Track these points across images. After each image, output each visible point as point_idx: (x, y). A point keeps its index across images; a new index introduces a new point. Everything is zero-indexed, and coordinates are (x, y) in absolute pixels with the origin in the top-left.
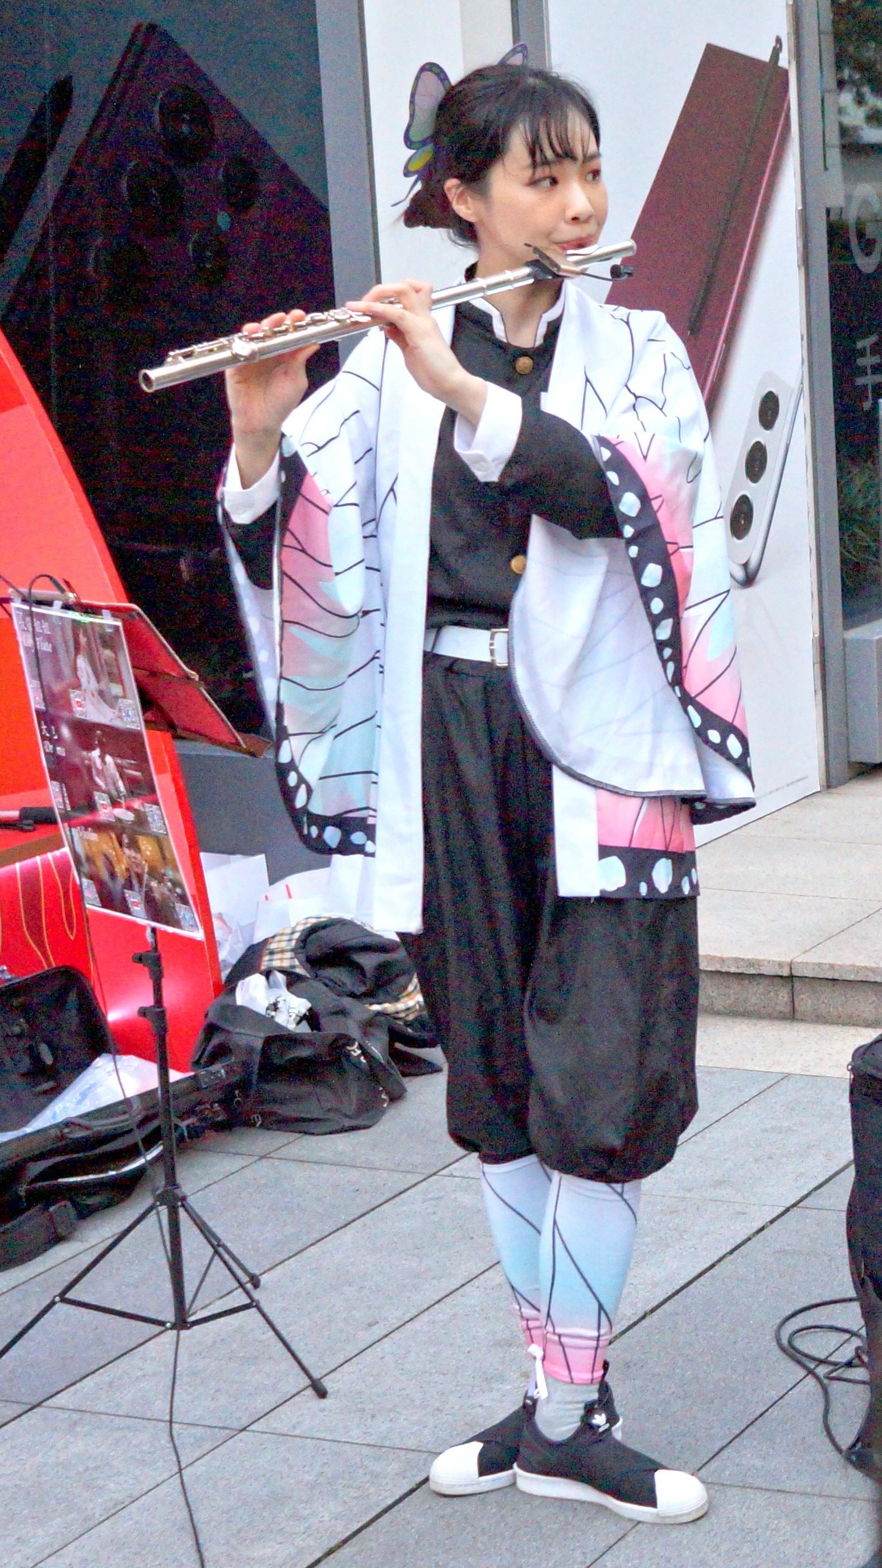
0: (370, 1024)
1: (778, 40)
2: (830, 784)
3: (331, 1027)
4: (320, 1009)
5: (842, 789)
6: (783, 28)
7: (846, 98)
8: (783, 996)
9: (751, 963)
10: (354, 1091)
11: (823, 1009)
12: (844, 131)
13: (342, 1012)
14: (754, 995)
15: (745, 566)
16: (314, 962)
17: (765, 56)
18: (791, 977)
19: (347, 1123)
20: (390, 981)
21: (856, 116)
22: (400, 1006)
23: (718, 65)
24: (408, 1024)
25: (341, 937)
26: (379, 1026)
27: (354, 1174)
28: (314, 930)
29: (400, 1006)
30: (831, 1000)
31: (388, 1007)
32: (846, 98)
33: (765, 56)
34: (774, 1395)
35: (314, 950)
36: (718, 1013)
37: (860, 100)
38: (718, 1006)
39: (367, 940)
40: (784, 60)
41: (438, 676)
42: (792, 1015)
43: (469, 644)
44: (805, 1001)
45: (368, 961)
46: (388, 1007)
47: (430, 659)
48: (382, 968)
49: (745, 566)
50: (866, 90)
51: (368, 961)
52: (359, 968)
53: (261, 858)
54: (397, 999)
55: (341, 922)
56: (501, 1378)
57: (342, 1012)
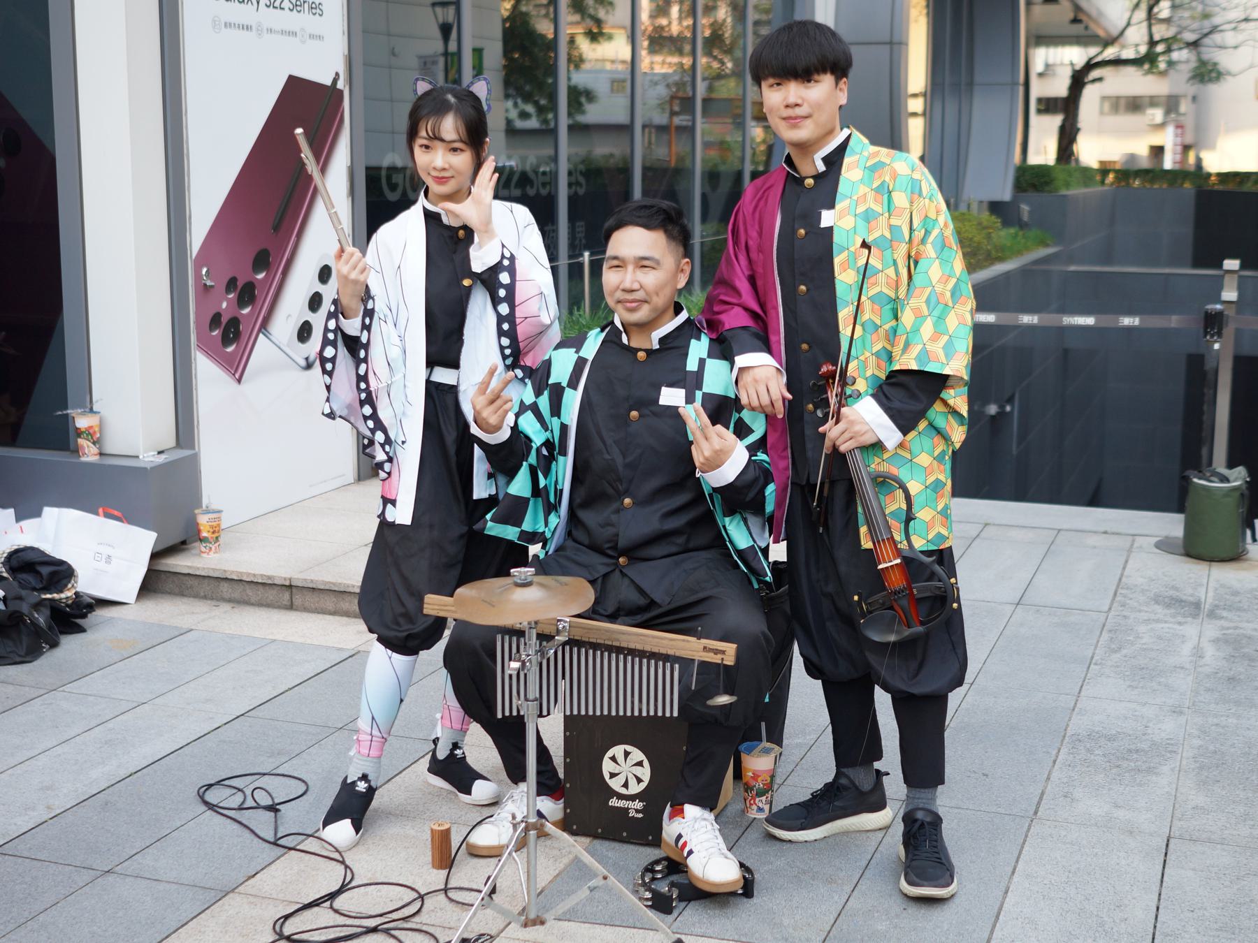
0: (38, 605)
1: (337, 74)
2: (360, 478)
3: (14, 606)
4: (9, 597)
5: (368, 482)
6: (341, 68)
7: (510, 104)
8: (287, 596)
9: (269, 578)
10: (25, 640)
11: (307, 604)
12: (509, 122)
13: (20, 598)
14: (271, 595)
15: (307, 359)
16: (13, 570)
17: (328, 82)
18: (290, 586)
19: (18, 659)
20: (59, 581)
21: (513, 114)
22: (63, 596)
23: (295, 86)
24: (68, 606)
25: (31, 557)
26: (45, 606)
27: (11, 688)
28: (17, 551)
29: (63, 596)
30: (310, 600)
31: (56, 596)
32: (510, 104)
33: (328, 82)
34: (179, 824)
35: (14, 563)
36: (253, 604)
37: (516, 105)
38: (253, 600)
39: (45, 559)
40: (340, 85)
41: (433, 389)
42: (291, 607)
43: (443, 376)
44: (298, 600)
45: (45, 571)
46: (56, 596)
47: (428, 382)
48: (53, 574)
49: (307, 359)
50: (519, 101)
51: (45, 571)
52: (38, 573)
53: (12, 511)
54: (61, 592)
55: (32, 549)
56: (34, 809)
57: (20, 598)
